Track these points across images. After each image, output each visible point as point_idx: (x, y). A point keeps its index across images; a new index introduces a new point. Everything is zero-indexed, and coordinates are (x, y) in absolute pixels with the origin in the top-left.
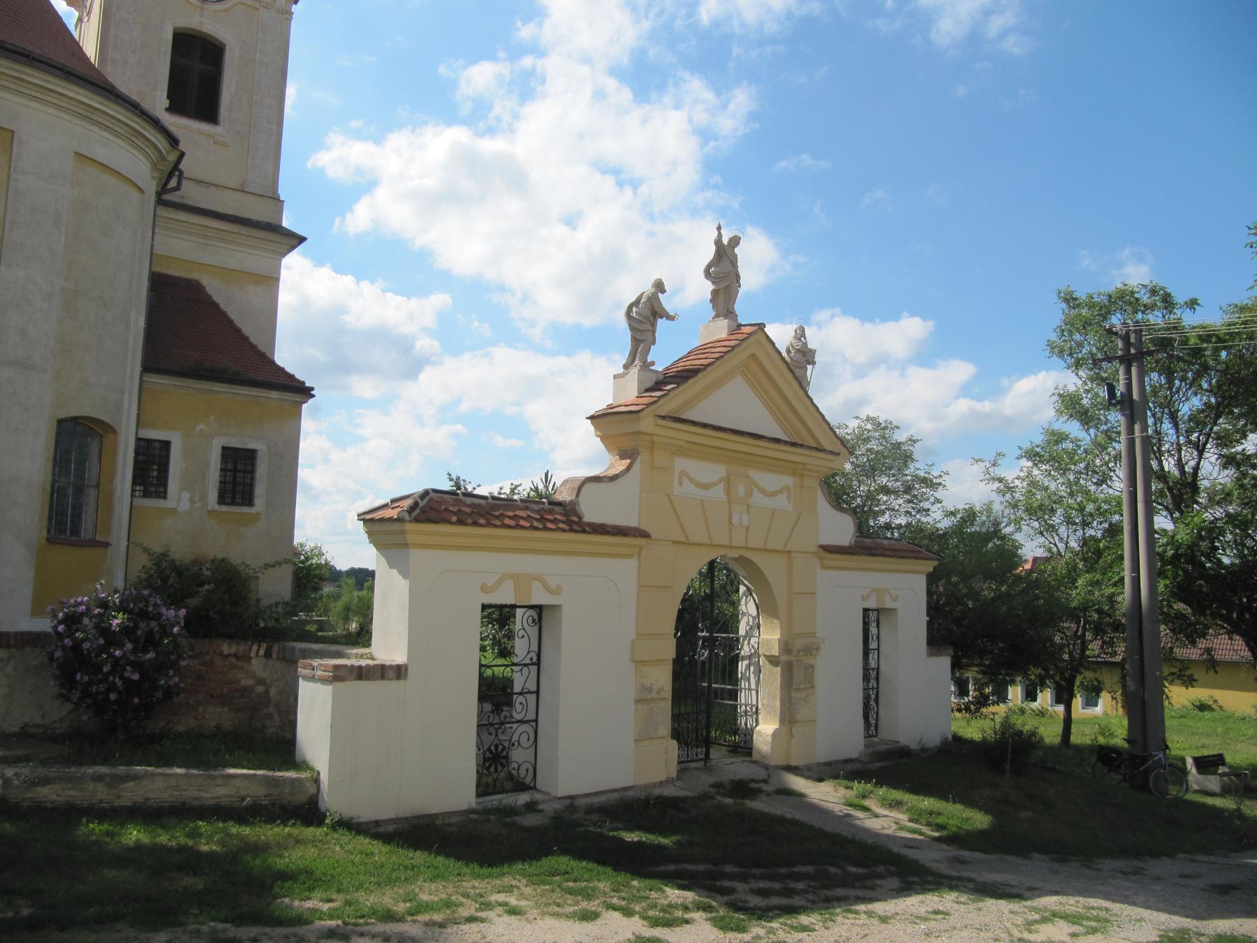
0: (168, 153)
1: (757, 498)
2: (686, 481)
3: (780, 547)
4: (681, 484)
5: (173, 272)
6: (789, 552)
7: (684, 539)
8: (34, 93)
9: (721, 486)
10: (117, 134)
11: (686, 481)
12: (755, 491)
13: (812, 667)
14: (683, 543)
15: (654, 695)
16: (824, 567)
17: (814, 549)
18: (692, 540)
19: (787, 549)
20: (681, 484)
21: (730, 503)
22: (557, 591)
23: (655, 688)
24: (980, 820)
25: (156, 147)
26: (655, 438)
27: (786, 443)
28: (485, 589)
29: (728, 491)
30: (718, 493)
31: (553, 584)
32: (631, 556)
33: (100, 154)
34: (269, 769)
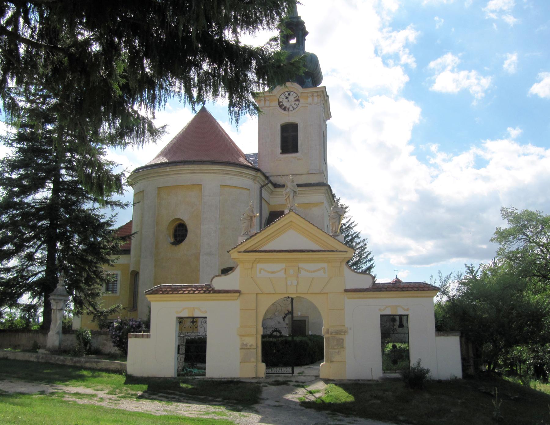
4: (260, 272)
33: (229, 183)
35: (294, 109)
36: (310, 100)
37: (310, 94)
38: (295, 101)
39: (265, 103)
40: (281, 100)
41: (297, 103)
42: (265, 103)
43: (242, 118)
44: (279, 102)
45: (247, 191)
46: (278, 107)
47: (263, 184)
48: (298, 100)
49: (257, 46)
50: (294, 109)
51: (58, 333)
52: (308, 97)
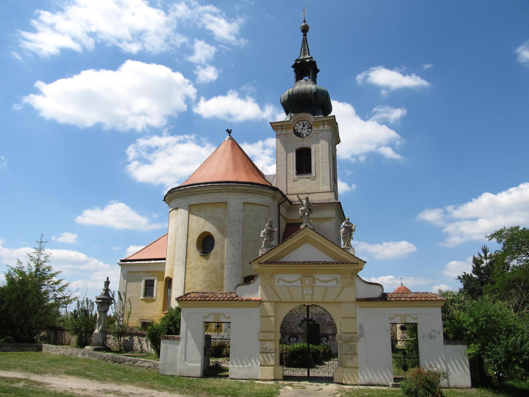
1: (318, 283)
2: (280, 281)
4: (278, 282)
5: (290, 222)
6: (340, 302)
7: (290, 300)
9: (299, 281)
10: (255, 194)
11: (280, 281)
13: (355, 346)
14: (291, 302)
15: (268, 351)
17: (354, 300)
18: (284, 300)
19: (338, 300)
20: (278, 282)
22: (416, 318)
23: (269, 348)
27: (333, 263)
28: (204, 317)
29: (301, 282)
30: (298, 283)
31: (227, 315)
33: (251, 200)
34: (378, 389)
35: (307, 135)
36: (321, 128)
38: (309, 128)
40: (296, 128)
41: (310, 130)
44: (294, 130)
45: (266, 208)
48: (311, 128)
50: (307, 135)
52: (319, 125)
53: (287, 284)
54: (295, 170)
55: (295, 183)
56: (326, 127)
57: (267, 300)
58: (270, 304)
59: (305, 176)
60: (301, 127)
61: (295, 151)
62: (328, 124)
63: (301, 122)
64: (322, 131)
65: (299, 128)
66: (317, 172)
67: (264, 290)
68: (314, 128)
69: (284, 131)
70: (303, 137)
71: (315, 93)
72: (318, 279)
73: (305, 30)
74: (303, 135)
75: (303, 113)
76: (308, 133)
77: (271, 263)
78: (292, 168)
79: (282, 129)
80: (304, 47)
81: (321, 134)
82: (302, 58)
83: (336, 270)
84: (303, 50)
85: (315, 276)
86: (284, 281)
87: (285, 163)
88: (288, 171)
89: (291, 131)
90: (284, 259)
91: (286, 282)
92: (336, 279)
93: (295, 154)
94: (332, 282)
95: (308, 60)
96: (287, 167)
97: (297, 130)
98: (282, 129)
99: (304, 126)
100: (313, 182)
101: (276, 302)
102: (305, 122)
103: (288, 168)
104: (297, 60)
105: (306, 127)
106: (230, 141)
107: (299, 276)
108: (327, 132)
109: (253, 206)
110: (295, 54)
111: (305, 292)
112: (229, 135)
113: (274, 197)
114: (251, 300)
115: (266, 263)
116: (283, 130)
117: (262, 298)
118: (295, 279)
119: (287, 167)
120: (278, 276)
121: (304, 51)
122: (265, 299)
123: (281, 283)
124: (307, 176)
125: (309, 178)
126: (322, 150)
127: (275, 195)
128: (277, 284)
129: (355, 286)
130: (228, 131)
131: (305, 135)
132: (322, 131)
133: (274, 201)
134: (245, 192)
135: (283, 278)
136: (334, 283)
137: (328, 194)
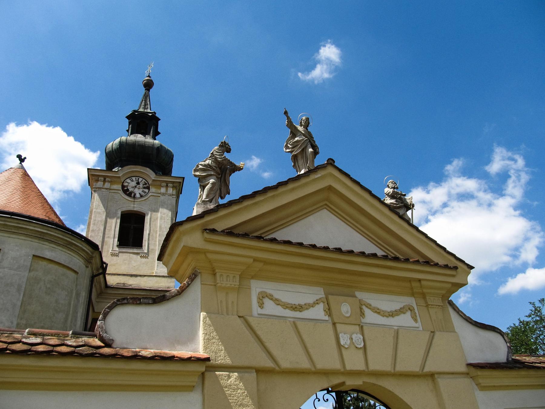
0: (93, 253)
1: (370, 317)
2: (267, 301)
3: (415, 368)
4: (261, 305)
6: (432, 376)
7: (305, 364)
8: (13, 231)
10: (59, 245)
11: (267, 301)
12: (367, 311)
16: (483, 388)
17: (463, 368)
18: (285, 364)
20: (261, 305)
21: (334, 324)
24: (503, 290)
25: (84, 250)
26: (210, 256)
29: (329, 311)
32: (190, 388)
33: (48, 254)
35: (141, 196)
36: (163, 190)
37: (164, 184)
38: (144, 188)
39: (104, 184)
40: (126, 184)
41: (147, 191)
42: (104, 184)
43: (59, 193)
44: (123, 187)
45: (73, 274)
46: (121, 192)
47: (95, 272)
48: (148, 188)
49: (31, 127)
50: (141, 196)
51: (428, 192)
52: (161, 186)
53: (288, 313)
54: (116, 240)
55: (115, 258)
56: (170, 191)
57: (228, 361)
58: (241, 379)
59: (131, 251)
60: (134, 184)
61: (119, 215)
62: (173, 187)
63: (134, 179)
64: (164, 194)
65: (131, 184)
66: (151, 247)
67: (218, 327)
68: (153, 189)
69: (107, 185)
70: (134, 197)
71: (158, 148)
72: (369, 306)
73: (149, 85)
74: (135, 195)
75: (141, 167)
76: (143, 194)
77: (245, 236)
78: (112, 236)
79: (104, 181)
80: (146, 101)
81: (162, 198)
82: (141, 110)
83: (410, 280)
84: (143, 104)
85: (360, 295)
86: (277, 302)
87: (102, 228)
88: (106, 239)
89: (119, 187)
90: (280, 235)
91: (286, 306)
92: (411, 309)
93: (119, 221)
94: (402, 316)
95: (150, 115)
96: (104, 234)
97: (127, 186)
98: (104, 181)
99: (138, 183)
100: (144, 260)
101: (259, 371)
102: (140, 179)
103: (106, 236)
104: (135, 111)
105: (141, 186)
106: (18, 177)
107: (318, 293)
108: (171, 197)
109: (51, 266)
110: (134, 104)
111: (344, 340)
112: (21, 163)
113: (88, 261)
114: (171, 359)
115: (229, 232)
116: (106, 184)
117: (212, 356)
118: (310, 299)
119: (104, 234)
120: (257, 287)
121: (145, 105)
122: (222, 357)
123: (270, 308)
124: (135, 251)
125: (137, 254)
126: (161, 219)
127: (92, 257)
128: (256, 309)
129: (454, 331)
130: (19, 157)
131: (138, 195)
132: (164, 194)
133: (87, 267)
134: (41, 237)
135: (277, 295)
136: (405, 320)
137: (166, 279)
